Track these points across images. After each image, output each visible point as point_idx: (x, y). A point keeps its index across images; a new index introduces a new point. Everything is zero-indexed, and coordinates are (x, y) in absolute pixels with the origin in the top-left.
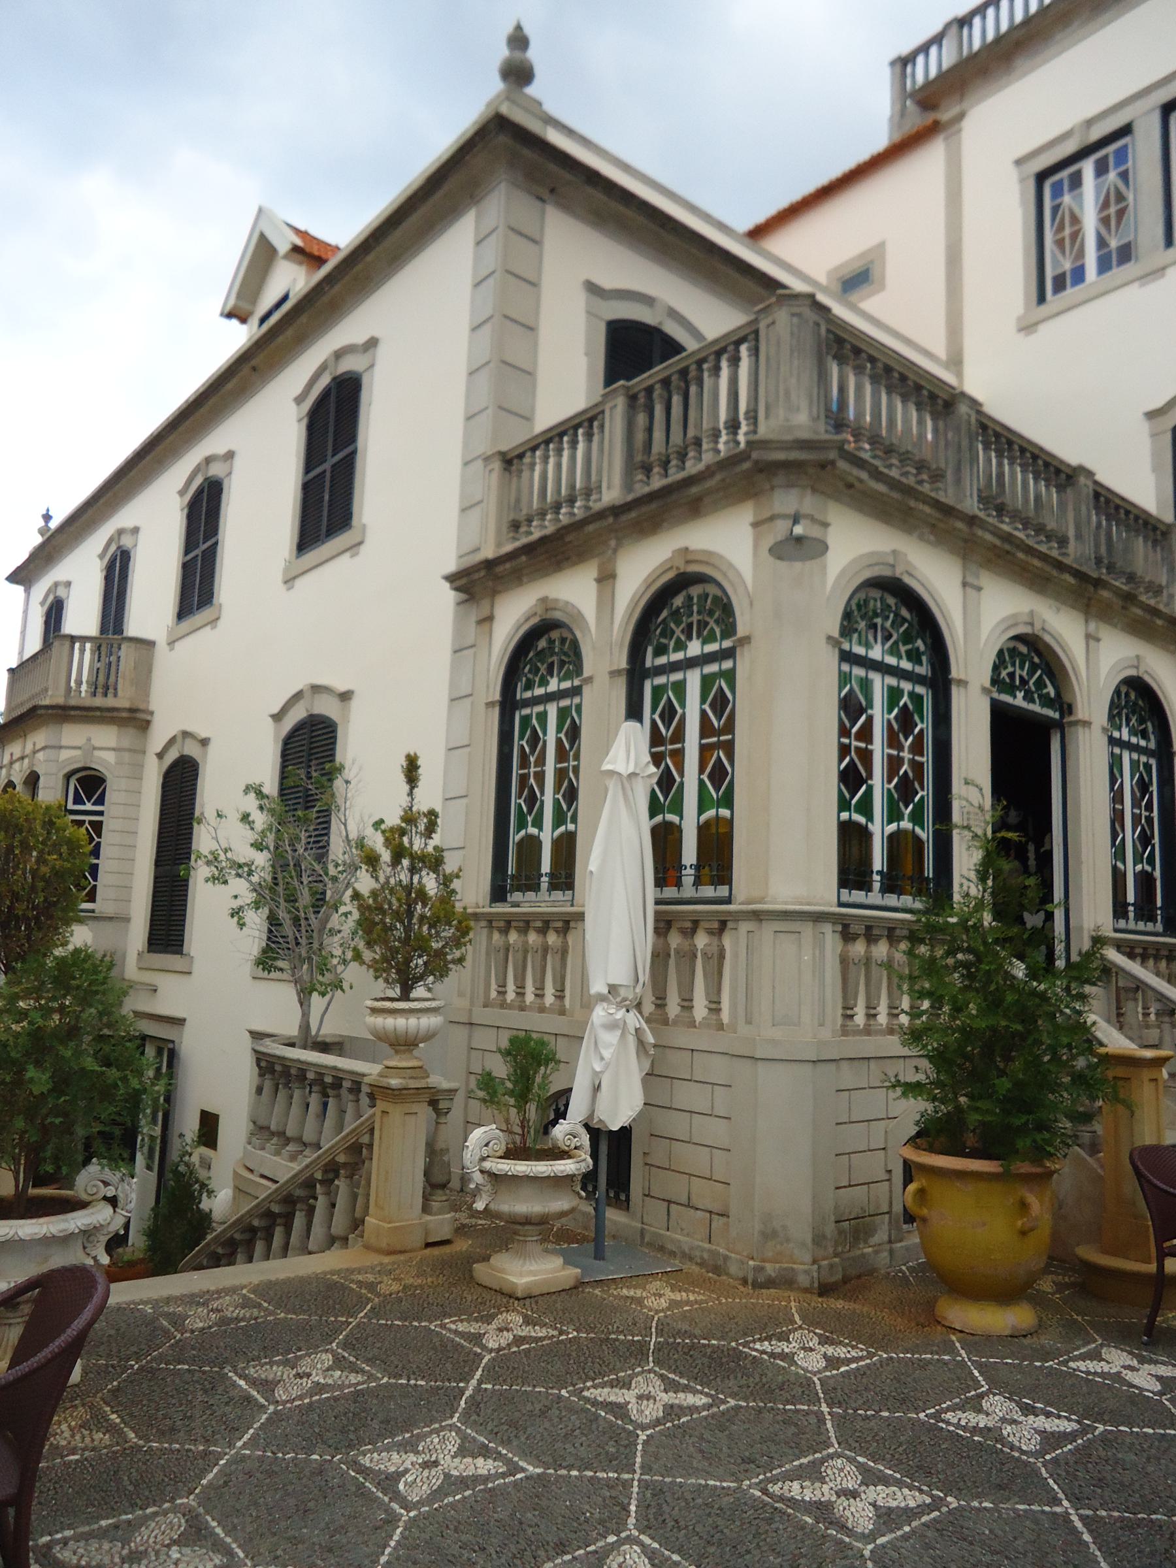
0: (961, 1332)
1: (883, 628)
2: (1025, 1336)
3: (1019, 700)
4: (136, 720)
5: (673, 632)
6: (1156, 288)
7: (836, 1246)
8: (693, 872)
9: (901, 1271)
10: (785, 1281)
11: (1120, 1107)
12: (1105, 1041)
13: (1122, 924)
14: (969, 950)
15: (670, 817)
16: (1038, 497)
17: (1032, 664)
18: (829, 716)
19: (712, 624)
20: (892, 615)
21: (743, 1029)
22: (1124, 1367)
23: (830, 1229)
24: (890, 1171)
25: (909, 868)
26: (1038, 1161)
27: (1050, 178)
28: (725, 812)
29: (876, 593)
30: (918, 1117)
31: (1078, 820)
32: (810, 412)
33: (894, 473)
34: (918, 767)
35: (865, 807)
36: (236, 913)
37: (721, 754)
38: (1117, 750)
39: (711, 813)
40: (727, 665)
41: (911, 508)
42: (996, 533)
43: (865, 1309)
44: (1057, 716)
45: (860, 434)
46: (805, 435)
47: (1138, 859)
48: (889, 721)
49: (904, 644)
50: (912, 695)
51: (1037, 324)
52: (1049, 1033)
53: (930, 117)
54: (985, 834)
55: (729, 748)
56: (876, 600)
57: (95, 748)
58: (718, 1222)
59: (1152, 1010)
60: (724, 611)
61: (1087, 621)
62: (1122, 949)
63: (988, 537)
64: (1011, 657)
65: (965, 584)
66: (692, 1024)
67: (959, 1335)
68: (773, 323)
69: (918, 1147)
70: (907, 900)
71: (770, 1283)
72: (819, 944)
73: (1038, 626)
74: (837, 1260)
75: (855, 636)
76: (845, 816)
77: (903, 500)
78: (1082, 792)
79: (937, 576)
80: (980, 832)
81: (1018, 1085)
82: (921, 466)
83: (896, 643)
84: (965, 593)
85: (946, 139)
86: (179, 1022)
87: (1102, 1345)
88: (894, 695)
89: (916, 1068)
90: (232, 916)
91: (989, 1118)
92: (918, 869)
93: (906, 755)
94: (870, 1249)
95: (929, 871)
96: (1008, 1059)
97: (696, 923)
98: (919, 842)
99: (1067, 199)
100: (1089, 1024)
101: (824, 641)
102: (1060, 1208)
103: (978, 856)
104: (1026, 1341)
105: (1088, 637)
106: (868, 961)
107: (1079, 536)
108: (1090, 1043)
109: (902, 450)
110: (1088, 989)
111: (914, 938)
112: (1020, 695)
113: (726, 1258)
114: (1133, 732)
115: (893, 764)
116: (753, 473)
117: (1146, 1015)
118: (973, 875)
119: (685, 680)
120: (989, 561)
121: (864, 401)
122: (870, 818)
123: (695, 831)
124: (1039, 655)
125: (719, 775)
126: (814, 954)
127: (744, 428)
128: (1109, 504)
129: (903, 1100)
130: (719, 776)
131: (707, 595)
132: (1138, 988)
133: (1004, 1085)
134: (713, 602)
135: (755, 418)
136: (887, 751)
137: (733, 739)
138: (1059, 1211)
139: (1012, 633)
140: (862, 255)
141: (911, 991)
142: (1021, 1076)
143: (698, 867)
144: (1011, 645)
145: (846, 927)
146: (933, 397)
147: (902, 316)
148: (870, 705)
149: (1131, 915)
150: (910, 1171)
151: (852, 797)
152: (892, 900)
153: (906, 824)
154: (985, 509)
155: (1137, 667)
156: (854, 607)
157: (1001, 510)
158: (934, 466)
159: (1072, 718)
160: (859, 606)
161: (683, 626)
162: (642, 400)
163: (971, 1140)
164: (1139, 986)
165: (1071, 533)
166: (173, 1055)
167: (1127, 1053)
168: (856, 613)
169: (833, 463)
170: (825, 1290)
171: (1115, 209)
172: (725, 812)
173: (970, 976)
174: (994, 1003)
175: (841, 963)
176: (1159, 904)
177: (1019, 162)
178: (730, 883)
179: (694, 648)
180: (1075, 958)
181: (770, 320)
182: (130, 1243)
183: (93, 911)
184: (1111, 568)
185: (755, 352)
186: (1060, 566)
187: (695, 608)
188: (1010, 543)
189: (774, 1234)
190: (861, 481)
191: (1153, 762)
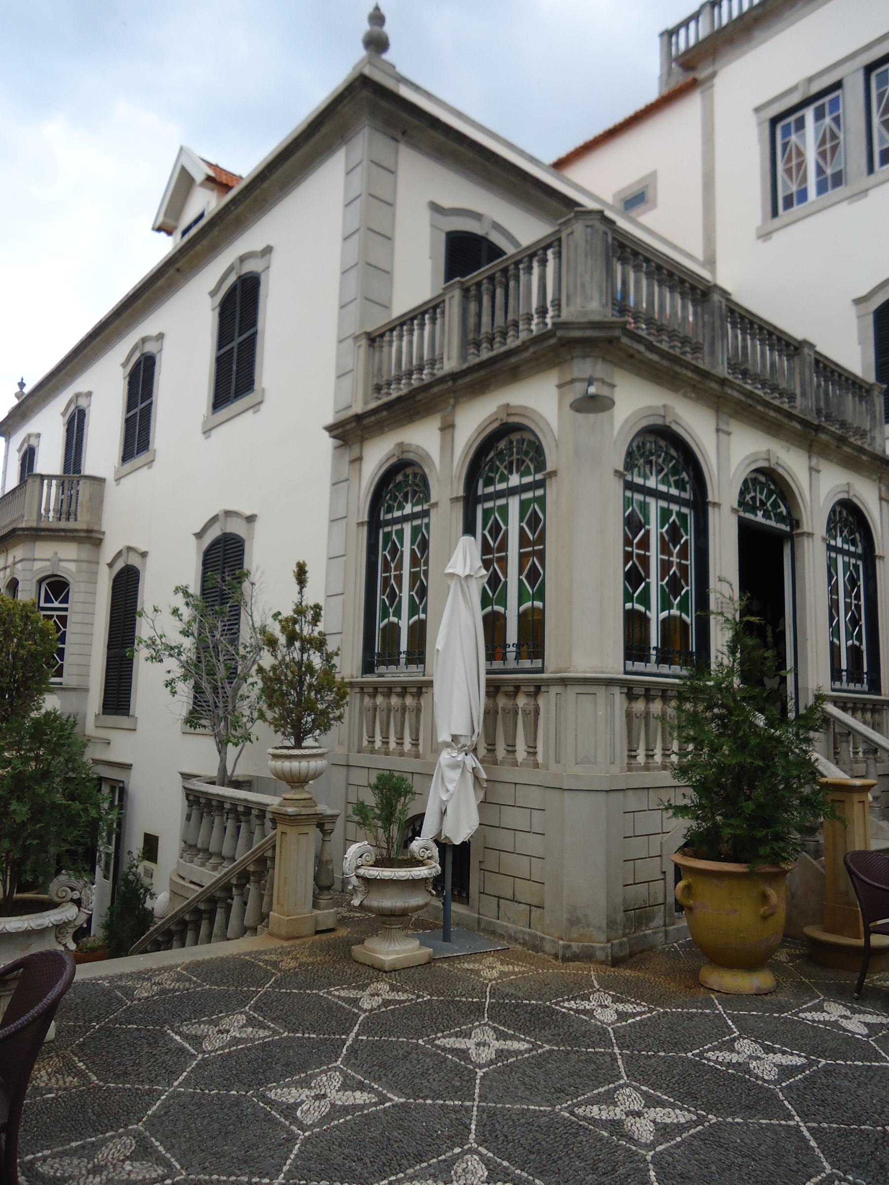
0: (718, 992)
3: (759, 517)
4: (92, 538)
5: (498, 468)
6: (861, 205)
8: (514, 649)
9: (673, 947)
10: (586, 956)
12: (825, 773)
13: (837, 685)
14: (723, 706)
16: (773, 364)
19: (527, 461)
20: (663, 454)
21: (553, 767)
22: (841, 1017)
23: (620, 916)
26: (775, 864)
27: (781, 122)
28: (538, 604)
29: (651, 438)
32: (600, 300)
33: (664, 346)
34: (683, 569)
35: (644, 599)
36: (169, 684)
37: (535, 560)
38: (833, 555)
39: (528, 604)
40: (539, 492)
41: (677, 373)
43: (647, 976)
44: (788, 529)
45: (639, 317)
46: (596, 318)
47: (849, 636)
50: (679, 514)
51: (771, 232)
52: (783, 767)
54: (734, 619)
55: (541, 555)
56: (651, 442)
57: (60, 560)
58: (536, 912)
59: (860, 749)
61: (810, 457)
62: (838, 704)
63: (736, 394)
64: (753, 485)
65: (718, 430)
66: (515, 764)
68: (572, 233)
69: (685, 854)
70: (676, 669)
73: (773, 461)
74: (625, 939)
76: (629, 606)
77: (671, 369)
79: (697, 424)
80: (730, 617)
81: (760, 806)
82: (685, 341)
83: (666, 475)
85: (702, 92)
86: (128, 767)
87: (824, 1000)
88: (665, 514)
89: (684, 795)
90: (167, 686)
92: (684, 644)
93: (675, 559)
95: (693, 647)
96: (752, 787)
97: (517, 689)
98: (685, 625)
99: (794, 138)
102: (793, 898)
103: (729, 635)
104: (767, 998)
105: (811, 469)
106: (647, 715)
107: (803, 394)
108: (814, 773)
110: (812, 734)
111: (681, 698)
113: (542, 939)
114: (845, 541)
115: (665, 566)
116: (558, 347)
118: (725, 650)
121: (641, 291)
122: (648, 607)
123: (516, 618)
124: (775, 483)
125: (534, 576)
126: (606, 710)
127: (550, 313)
128: (826, 368)
130: (534, 576)
131: (523, 440)
132: (849, 733)
135: (559, 305)
136: (660, 556)
138: (791, 901)
139: (754, 467)
140: (639, 182)
141: (680, 736)
142: (762, 800)
143: (519, 646)
144: (754, 475)
145: (630, 689)
146: (693, 288)
147: (670, 227)
148: (647, 522)
149: (844, 678)
151: (634, 592)
152: (665, 669)
153: (675, 612)
156: (635, 448)
157: (745, 374)
158: (694, 341)
159: (799, 531)
160: (638, 447)
163: (725, 847)
164: (851, 732)
165: (798, 391)
166: (123, 792)
167: (843, 781)
171: (830, 145)
172: (538, 604)
173: (724, 726)
174: (742, 746)
176: (865, 670)
177: (757, 110)
179: (515, 480)
180: (802, 711)
181: (569, 230)
182: (92, 934)
183: (61, 684)
184: (828, 417)
185: (558, 255)
186: (789, 415)
187: (515, 450)
188: (753, 399)
190: (640, 352)
191: (860, 563)
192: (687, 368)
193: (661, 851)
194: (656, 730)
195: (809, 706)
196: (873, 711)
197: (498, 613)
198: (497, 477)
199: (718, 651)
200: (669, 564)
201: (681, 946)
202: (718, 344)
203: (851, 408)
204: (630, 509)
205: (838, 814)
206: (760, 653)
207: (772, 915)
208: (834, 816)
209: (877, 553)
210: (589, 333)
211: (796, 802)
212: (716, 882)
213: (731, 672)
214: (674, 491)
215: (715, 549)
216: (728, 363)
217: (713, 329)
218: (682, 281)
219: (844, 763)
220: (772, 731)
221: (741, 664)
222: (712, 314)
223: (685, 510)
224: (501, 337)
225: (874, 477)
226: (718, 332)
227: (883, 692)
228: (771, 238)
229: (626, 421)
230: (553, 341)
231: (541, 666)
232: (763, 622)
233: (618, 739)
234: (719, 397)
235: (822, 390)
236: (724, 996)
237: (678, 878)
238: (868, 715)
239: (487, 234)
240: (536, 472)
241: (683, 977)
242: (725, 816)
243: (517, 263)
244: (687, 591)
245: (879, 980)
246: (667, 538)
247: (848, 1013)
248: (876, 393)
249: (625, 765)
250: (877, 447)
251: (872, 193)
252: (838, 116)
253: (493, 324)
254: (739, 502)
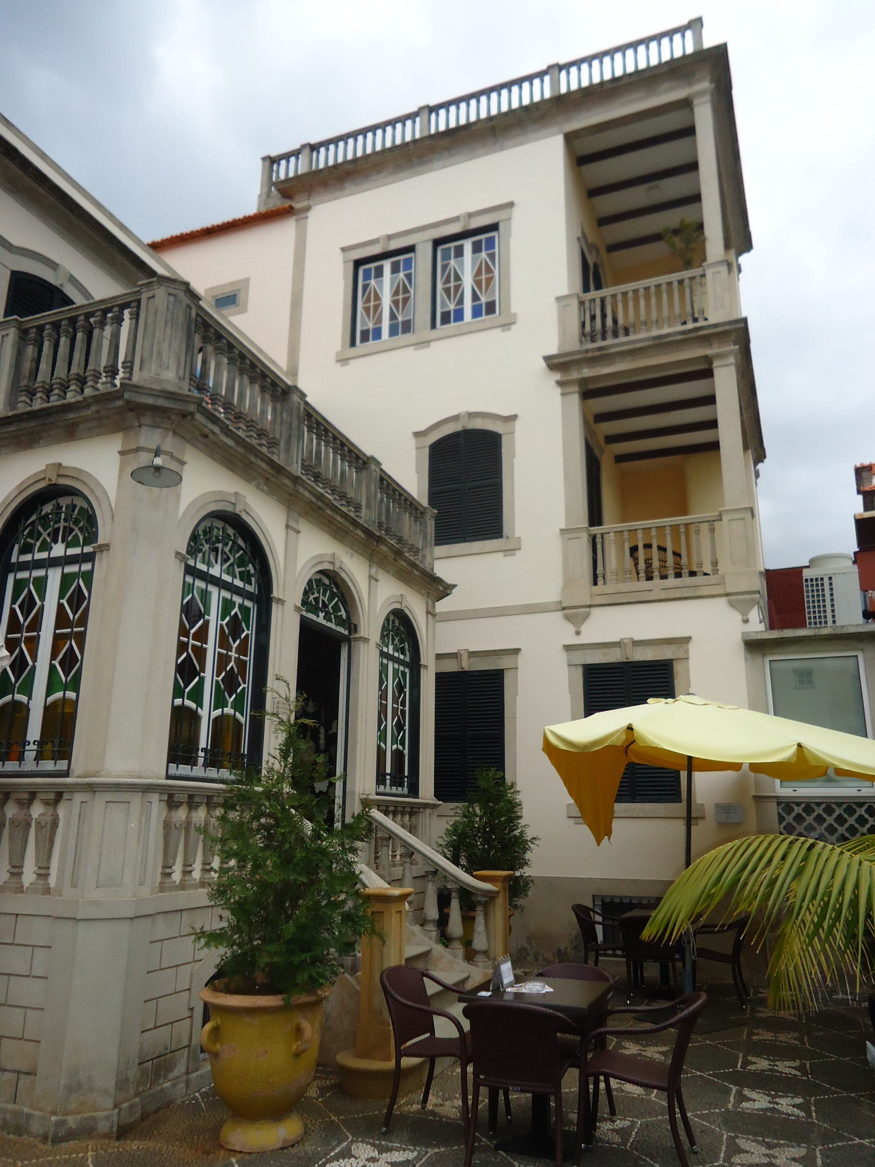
0: (240, 1152)
1: (223, 552)
2: (293, 1146)
3: (320, 619)
5: (40, 534)
6: (424, 353)
7: (138, 1085)
8: (35, 747)
9: (195, 1098)
10: (86, 1131)
11: (375, 939)
12: (366, 882)
13: (382, 789)
14: (270, 815)
15: (19, 697)
17: (332, 592)
18: (172, 617)
19: (77, 530)
20: (231, 543)
21: (68, 893)
23: (133, 1072)
24: (192, 1009)
25: (228, 747)
26: (312, 991)
27: (363, 265)
28: (71, 695)
29: (219, 524)
30: (218, 962)
31: (356, 712)
32: (177, 372)
33: (240, 433)
34: (242, 665)
35: (197, 695)
37: (73, 643)
38: (385, 661)
39: (59, 695)
40: (87, 567)
41: (251, 463)
44: (346, 632)
45: (217, 399)
46: (171, 388)
47: (394, 741)
48: (221, 626)
49: (238, 567)
50: (241, 607)
51: (349, 359)
52: (327, 883)
53: (287, 203)
55: (81, 639)
56: (219, 529)
58: (24, 1081)
59: (398, 852)
60: (89, 520)
61: (370, 566)
63: (307, 494)
64: (317, 586)
66: (20, 889)
67: (240, 1156)
68: (154, 297)
69: (216, 990)
70: (225, 773)
71: (72, 1135)
72: (146, 813)
73: (337, 565)
74: (137, 1100)
75: (200, 555)
76: (178, 702)
77: (245, 455)
78: (360, 687)
80: (285, 718)
81: (302, 928)
82: (261, 434)
83: (232, 565)
85: (296, 220)
87: (352, 1142)
88: (227, 605)
89: (221, 917)
92: (235, 747)
93: (233, 654)
95: (245, 749)
96: (295, 906)
97: (33, 795)
98: (238, 724)
99: (373, 282)
100: (357, 872)
101: (173, 555)
102: (327, 1020)
103: (282, 737)
104: (293, 1151)
105: (371, 577)
106: (188, 824)
107: (368, 506)
108: (352, 878)
110: (358, 844)
111: (228, 806)
112: (322, 615)
113: (29, 1117)
114: (396, 649)
115: (223, 661)
116: (122, 411)
117: (394, 856)
118: (277, 754)
119: (46, 577)
120: (307, 513)
121: (220, 375)
122: (200, 704)
123: (42, 711)
124: (337, 587)
125: (70, 662)
127: (121, 375)
128: (388, 487)
129: (206, 950)
131: (75, 506)
132: (390, 838)
133: (289, 929)
134: (79, 513)
135: (132, 368)
136: (218, 650)
137: (85, 631)
138: (325, 1029)
140: (231, 284)
141: (222, 851)
142: (304, 920)
143: (41, 743)
144: (318, 577)
145: (171, 796)
146: (274, 385)
147: (259, 327)
148: (208, 611)
149: (388, 782)
150: (208, 1011)
152: (212, 773)
153: (229, 710)
154: (306, 475)
155: (401, 603)
156: (201, 532)
157: (317, 477)
160: (205, 532)
162: (32, 335)
163: (260, 977)
164: (391, 836)
165: (364, 503)
167: (383, 892)
168: (202, 537)
169: (192, 414)
170: (123, 1132)
172: (71, 695)
173: (269, 838)
174: (286, 860)
176: (406, 774)
177: (344, 250)
178: (69, 759)
179: (58, 550)
180: (349, 820)
181: (150, 294)
184: (388, 531)
185: (136, 317)
186: (355, 523)
187: (63, 516)
188: (323, 501)
190: (214, 433)
191: (407, 670)
193: (191, 983)
194: (197, 843)
195: (356, 814)
196: (412, 814)
197: (20, 703)
198: (38, 544)
200: (228, 659)
201: (204, 1095)
202: (294, 444)
203: (407, 525)
204: (190, 596)
209: (422, 662)
210: (160, 402)
211: (338, 919)
212: (248, 1020)
213: (281, 778)
214: (238, 583)
215: (275, 647)
216: (302, 464)
217: (290, 428)
218: (264, 376)
220: (319, 842)
224: (60, 390)
225: (424, 592)
226: (295, 432)
227: (420, 796)
231: (66, 769)
232: (317, 725)
234: (290, 495)
236: (246, 1157)
237: (206, 1020)
239: (62, 285)
240: (84, 545)
241: (201, 1138)
242: (263, 939)
244: (244, 688)
245: (406, 1104)
246: (227, 631)
247: (375, 1154)
248: (428, 516)
250: (427, 565)
252: (410, 274)
253: (52, 374)
254: (303, 601)
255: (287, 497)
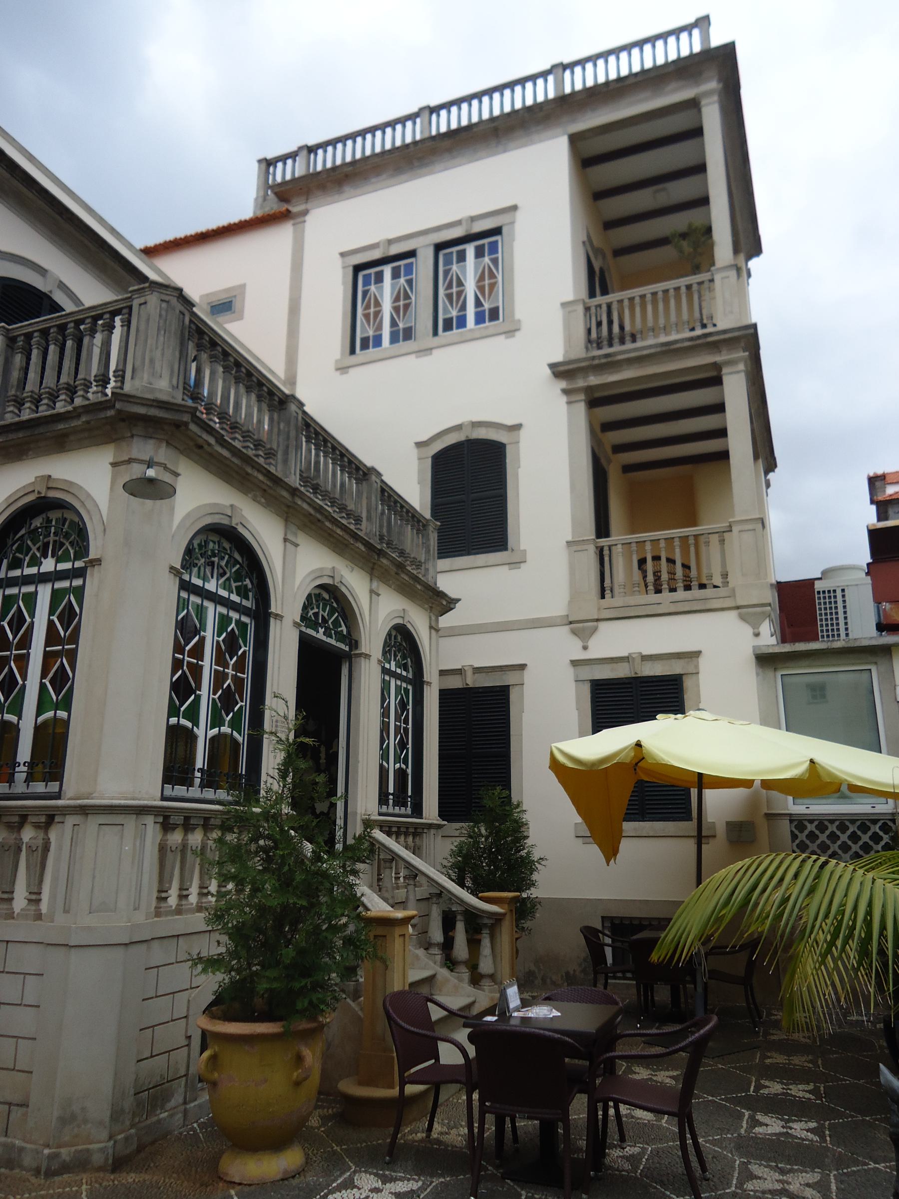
0: (240, 1184)
1: (219, 566)
2: (293, 1177)
3: (320, 635)
6: (425, 360)
8: (25, 769)
10: (80, 1164)
11: (378, 963)
12: (369, 905)
13: (384, 809)
14: (269, 837)
16: (343, 485)
17: (332, 607)
20: (227, 557)
21: (61, 919)
22: (372, 1191)
23: (128, 1103)
24: (189, 1037)
26: (313, 1019)
27: (363, 270)
28: (62, 714)
32: (171, 381)
33: (237, 444)
34: (239, 682)
35: (193, 714)
38: (387, 678)
39: (50, 714)
40: (77, 582)
41: (248, 474)
42: (311, 504)
43: (155, 1178)
46: (164, 398)
48: (218, 642)
53: (284, 207)
54: (288, 739)
55: (72, 656)
56: (214, 543)
58: (17, 1113)
61: (371, 580)
62: (384, 829)
63: (305, 506)
64: (317, 601)
65: (286, 540)
68: (145, 303)
70: (222, 794)
71: (66, 1168)
73: (337, 580)
74: (133, 1131)
75: (195, 570)
76: (174, 720)
77: (239, 466)
79: (265, 531)
80: (283, 737)
81: (301, 952)
82: (258, 444)
84: (285, 546)
85: (294, 225)
87: (355, 1172)
88: (224, 621)
89: (218, 942)
91: (275, 985)
92: (232, 766)
93: (230, 671)
94: (166, 1114)
96: (294, 930)
100: (359, 895)
103: (281, 756)
104: (294, 1182)
105: (372, 592)
106: (184, 846)
107: (369, 518)
108: (354, 902)
109: (244, 429)
110: (360, 866)
111: (226, 828)
112: (321, 630)
113: (21, 1150)
115: (219, 678)
116: (116, 421)
117: (397, 878)
118: (276, 774)
119: (36, 592)
121: (215, 384)
122: (196, 723)
124: (337, 602)
125: (61, 680)
126: (134, 845)
127: (112, 384)
130: (60, 681)
131: (65, 520)
133: (288, 954)
135: (123, 377)
136: (214, 667)
137: (46, 645)
138: (326, 1057)
139: (318, 582)
141: (220, 874)
143: (31, 765)
144: (317, 591)
145: (166, 818)
146: (271, 394)
147: (255, 335)
149: (391, 802)
151: (181, 705)
152: (209, 794)
153: (225, 729)
156: (196, 546)
157: (316, 488)
158: (268, 446)
159: (357, 652)
160: (200, 545)
161: (40, 544)
164: (394, 857)
165: (364, 515)
167: (385, 915)
169: (186, 424)
170: (118, 1164)
171: (403, 303)
172: (62, 714)
173: (268, 860)
174: (286, 884)
175: (159, 851)
176: (410, 794)
177: (343, 255)
179: (48, 565)
180: (350, 841)
181: (142, 300)
184: (389, 544)
185: (127, 324)
186: (355, 536)
187: (53, 530)
189: (73, 1117)
190: (209, 444)
191: (410, 687)
192: (258, 471)
193: (188, 1010)
196: (415, 835)
198: (27, 559)
199: (268, 774)
200: (225, 676)
203: (409, 539)
205: (380, 954)
206: (311, 777)
207: (306, 1079)
208: (376, 956)
210: (153, 412)
213: (280, 798)
214: (235, 598)
216: (300, 475)
217: (288, 438)
219: (387, 891)
221: (291, 791)
222: (288, 423)
223: (245, 619)
225: (426, 606)
228: (347, 373)
229: (188, 515)
230: (111, 413)
232: (317, 744)
233: (146, 877)
235: (385, 517)
236: (246, 1189)
237: (203, 1049)
238: (410, 839)
243: (78, 323)
247: (379, 1184)
248: (431, 529)
249: (153, 909)
251: (435, 352)
255: (286, 509)
